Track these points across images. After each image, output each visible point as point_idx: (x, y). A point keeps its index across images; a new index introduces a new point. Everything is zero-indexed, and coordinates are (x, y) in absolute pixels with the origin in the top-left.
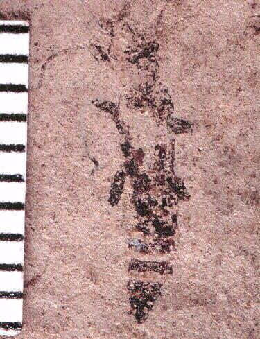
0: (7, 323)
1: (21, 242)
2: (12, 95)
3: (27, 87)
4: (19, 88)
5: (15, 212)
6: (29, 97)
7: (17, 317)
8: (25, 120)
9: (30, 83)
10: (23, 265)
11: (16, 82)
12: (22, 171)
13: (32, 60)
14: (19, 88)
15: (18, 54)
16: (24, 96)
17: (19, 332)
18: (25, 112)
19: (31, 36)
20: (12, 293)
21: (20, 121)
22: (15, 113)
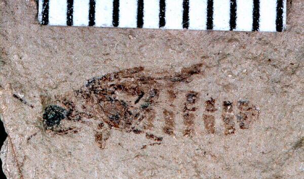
0: (48, 14)
1: (112, 25)
2: (228, 18)
3: (234, 30)
4: (233, 23)
5: (181, 20)
6: (226, 32)
7: (52, 21)
8: (208, 28)
9: (237, 33)
10: (94, 26)
11: (238, 22)
12: (122, 23)
13: (91, 28)
14: (233, 23)
15: (137, 20)
16: (227, 27)
17: (41, 23)
18: (215, 28)
19: (110, 28)
20: (72, 17)
21: (207, 25)
22: (213, 21)
